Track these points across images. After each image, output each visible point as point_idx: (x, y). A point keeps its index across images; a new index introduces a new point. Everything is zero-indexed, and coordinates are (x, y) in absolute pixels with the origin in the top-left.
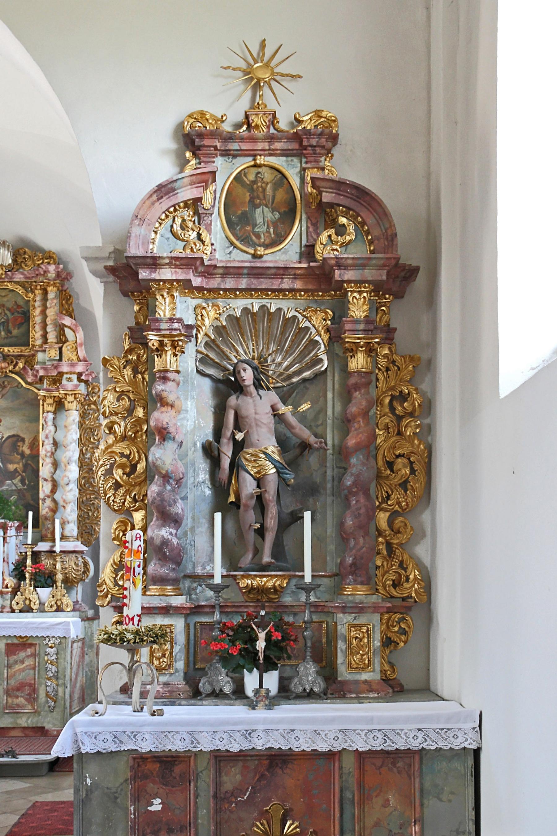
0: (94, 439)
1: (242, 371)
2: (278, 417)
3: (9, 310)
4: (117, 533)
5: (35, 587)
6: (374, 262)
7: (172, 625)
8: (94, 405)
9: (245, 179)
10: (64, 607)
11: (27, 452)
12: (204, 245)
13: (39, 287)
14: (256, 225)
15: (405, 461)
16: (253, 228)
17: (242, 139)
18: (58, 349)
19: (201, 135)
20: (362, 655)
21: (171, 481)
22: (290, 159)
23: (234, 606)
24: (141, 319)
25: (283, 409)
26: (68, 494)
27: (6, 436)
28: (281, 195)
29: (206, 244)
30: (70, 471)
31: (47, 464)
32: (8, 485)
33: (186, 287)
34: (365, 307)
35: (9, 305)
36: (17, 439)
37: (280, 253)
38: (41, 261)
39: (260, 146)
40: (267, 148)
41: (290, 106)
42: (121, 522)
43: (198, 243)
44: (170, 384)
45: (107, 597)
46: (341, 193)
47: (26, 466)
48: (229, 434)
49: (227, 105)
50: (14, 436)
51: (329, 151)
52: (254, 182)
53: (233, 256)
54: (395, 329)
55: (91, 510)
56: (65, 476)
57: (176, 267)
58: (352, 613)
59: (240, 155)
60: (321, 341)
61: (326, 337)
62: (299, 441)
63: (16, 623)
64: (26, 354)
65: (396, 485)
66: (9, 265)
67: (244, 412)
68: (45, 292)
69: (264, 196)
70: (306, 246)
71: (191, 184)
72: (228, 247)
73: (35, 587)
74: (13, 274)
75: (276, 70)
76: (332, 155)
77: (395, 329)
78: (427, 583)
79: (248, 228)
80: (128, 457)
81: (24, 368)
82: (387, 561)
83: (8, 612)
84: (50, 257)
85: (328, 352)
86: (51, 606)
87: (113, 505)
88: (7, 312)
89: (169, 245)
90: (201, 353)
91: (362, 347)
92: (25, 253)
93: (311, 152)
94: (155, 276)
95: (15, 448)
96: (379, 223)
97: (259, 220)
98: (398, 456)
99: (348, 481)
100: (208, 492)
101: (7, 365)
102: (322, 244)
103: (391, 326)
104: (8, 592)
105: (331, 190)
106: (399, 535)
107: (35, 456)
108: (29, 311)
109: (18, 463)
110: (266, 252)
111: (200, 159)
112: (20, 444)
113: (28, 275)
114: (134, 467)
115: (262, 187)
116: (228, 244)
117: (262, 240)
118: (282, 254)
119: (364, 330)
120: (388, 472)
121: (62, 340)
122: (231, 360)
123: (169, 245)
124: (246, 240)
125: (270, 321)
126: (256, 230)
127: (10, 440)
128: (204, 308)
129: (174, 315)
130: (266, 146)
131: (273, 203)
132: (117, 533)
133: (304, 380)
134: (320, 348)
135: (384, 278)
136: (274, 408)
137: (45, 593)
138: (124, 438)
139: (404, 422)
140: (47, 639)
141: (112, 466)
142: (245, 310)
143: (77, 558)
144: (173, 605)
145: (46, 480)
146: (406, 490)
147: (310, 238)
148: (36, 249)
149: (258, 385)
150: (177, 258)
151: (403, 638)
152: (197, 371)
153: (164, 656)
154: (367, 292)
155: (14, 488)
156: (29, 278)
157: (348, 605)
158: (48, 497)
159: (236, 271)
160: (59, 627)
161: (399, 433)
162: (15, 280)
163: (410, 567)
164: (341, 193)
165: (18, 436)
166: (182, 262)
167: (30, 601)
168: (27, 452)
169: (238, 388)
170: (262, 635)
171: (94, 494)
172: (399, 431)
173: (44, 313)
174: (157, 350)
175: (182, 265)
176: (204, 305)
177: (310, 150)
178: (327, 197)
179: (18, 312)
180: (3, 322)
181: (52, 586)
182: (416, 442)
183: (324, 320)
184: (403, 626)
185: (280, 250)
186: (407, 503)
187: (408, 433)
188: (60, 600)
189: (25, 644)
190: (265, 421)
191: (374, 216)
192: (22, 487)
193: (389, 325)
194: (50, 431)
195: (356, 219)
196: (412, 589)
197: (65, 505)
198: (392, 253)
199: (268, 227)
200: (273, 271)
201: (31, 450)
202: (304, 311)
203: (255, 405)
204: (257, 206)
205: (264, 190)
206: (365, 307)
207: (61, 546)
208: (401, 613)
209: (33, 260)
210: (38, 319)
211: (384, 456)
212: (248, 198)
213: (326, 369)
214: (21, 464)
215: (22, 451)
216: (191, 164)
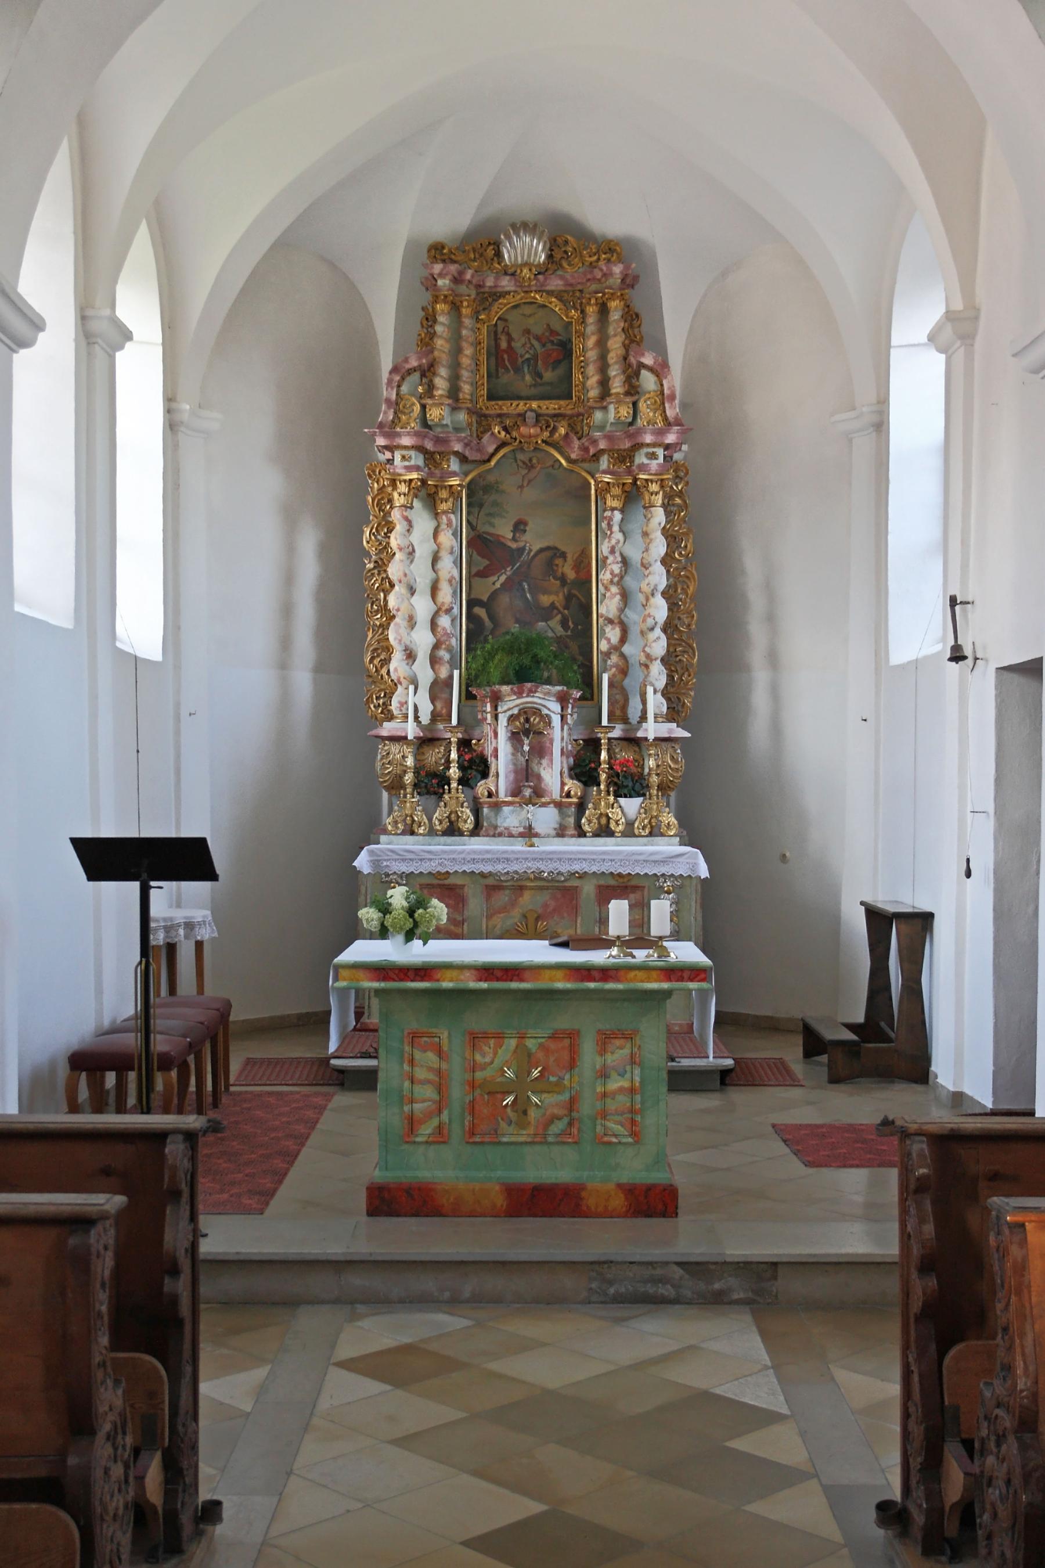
0: (680, 554)
3: (538, 338)
5: (617, 795)
8: (680, 497)
10: (663, 829)
11: (571, 575)
13: (593, 301)
18: (631, 406)
26: (654, 644)
27: (536, 548)
30: (657, 607)
35: (538, 330)
36: (554, 554)
38: (595, 258)
47: (569, 598)
50: (548, 548)
55: (677, 671)
56: (649, 615)
63: (613, 852)
64: (569, 412)
66: (539, 265)
68: (604, 310)
73: (617, 795)
74: (546, 279)
81: (567, 434)
83: (572, 836)
84: (611, 251)
86: (644, 828)
88: (535, 343)
92: (566, 242)
95: (550, 567)
104: (570, 804)
107: (584, 584)
108: (570, 341)
109: (557, 594)
112: (559, 561)
113: (573, 281)
121: (633, 390)
127: (543, 555)
137: (631, 805)
140: (662, 880)
148: (585, 236)
156: (571, 285)
160: (680, 859)
162: (549, 288)
165: (556, 548)
167: (609, 818)
168: (571, 575)
171: (680, 645)
173: (602, 344)
179: (552, 342)
180: (528, 359)
181: (644, 795)
188: (656, 817)
189: (626, 887)
192: (564, 633)
194: (618, 542)
197: (648, 663)
201: (577, 572)
207: (655, 731)
209: (581, 256)
210: (592, 355)
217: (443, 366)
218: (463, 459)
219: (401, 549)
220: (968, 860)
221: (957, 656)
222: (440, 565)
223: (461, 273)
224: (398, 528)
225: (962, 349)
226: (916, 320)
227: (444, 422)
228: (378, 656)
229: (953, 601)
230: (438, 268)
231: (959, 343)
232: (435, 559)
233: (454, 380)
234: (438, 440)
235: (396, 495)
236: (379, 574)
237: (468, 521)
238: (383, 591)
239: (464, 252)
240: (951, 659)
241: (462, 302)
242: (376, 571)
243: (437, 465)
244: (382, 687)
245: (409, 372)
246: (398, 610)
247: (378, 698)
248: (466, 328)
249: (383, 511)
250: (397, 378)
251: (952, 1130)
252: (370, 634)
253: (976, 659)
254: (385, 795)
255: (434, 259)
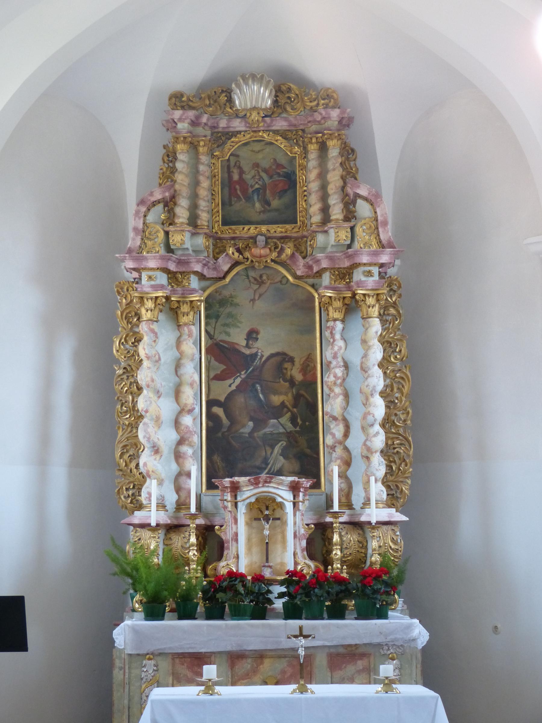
3: (265, 171)
8: (394, 307)
13: (314, 140)
18: (349, 230)
26: (373, 439)
31: (337, 396)
32: (273, 426)
35: (266, 164)
47: (297, 398)
55: (395, 462)
68: (323, 148)
81: (293, 255)
84: (329, 97)
92: (289, 90)
101: (268, 251)
108: (294, 173)
109: (286, 394)
112: (287, 365)
127: (273, 360)
143: (395, 533)
145: (335, 419)
148: (305, 84)
155: (282, 430)
156: (295, 126)
158: (340, 443)
162: (274, 128)
165: (284, 354)
168: (299, 377)
179: (279, 175)
180: (257, 189)
194: (340, 348)
201: (304, 375)
209: (303, 101)
210: (314, 186)
214: (290, 395)
215: (291, 376)
217: (183, 197)
218: (201, 277)
219: (148, 358)
222: (182, 371)
223: (198, 117)
224: (145, 338)
227: (185, 246)
228: (127, 452)
230: (177, 114)
232: (178, 366)
233: (194, 208)
234: (180, 262)
235: (143, 311)
236: (128, 379)
237: (206, 331)
238: (131, 393)
239: (201, 98)
241: (199, 142)
242: (125, 377)
243: (179, 283)
244: (131, 479)
245: (154, 204)
246: (146, 411)
247: (127, 489)
248: (203, 164)
249: (131, 323)
250: (143, 209)
252: (120, 433)
255: (175, 107)
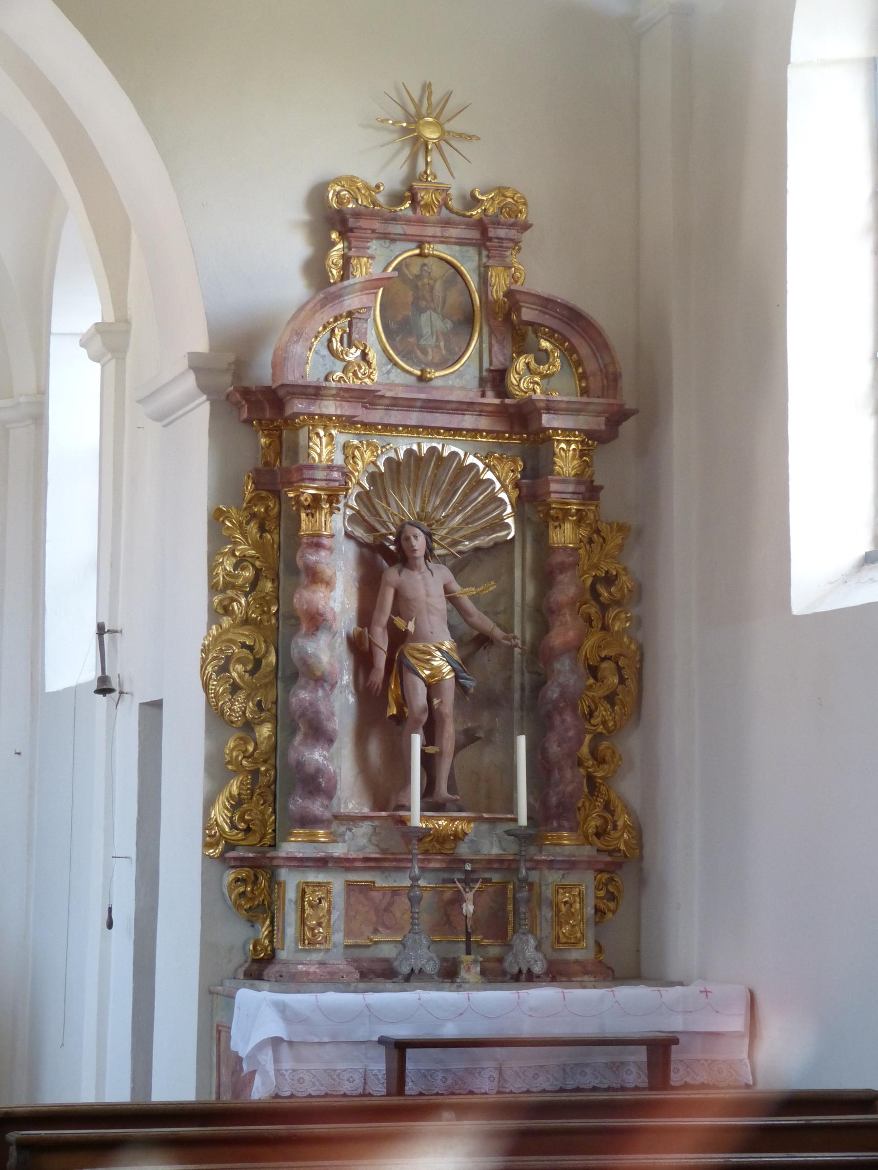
1: (412, 538)
2: (452, 599)
4: (234, 754)
6: (592, 407)
7: (329, 883)
9: (406, 271)
12: (370, 367)
14: (422, 336)
15: (613, 665)
16: (418, 340)
17: (408, 221)
19: (357, 214)
20: (573, 926)
21: (326, 685)
22: (465, 248)
23: (395, 860)
24: (271, 457)
25: (455, 586)
28: (454, 297)
29: (373, 366)
33: (347, 422)
34: (575, 462)
37: (453, 376)
39: (430, 231)
40: (439, 234)
41: (460, 174)
42: (241, 739)
43: (364, 367)
44: (323, 553)
45: (218, 845)
46: (548, 311)
48: (384, 620)
49: (374, 166)
51: (516, 242)
52: (419, 277)
53: (392, 377)
54: (601, 488)
57: (343, 399)
58: (560, 869)
59: (400, 240)
60: (507, 500)
61: (515, 494)
62: (476, 633)
65: (600, 698)
67: (410, 593)
69: (433, 300)
70: (489, 371)
71: (361, 291)
72: (387, 365)
75: (447, 127)
76: (520, 249)
77: (601, 488)
78: (638, 832)
79: (412, 340)
80: (251, 648)
82: (590, 800)
85: (518, 514)
87: (230, 715)
89: (325, 365)
90: (352, 508)
91: (572, 516)
93: (497, 244)
94: (314, 409)
96: (595, 355)
97: (426, 330)
98: (603, 659)
99: (553, 692)
100: (352, 699)
102: (518, 373)
103: (595, 484)
105: (535, 307)
106: (606, 766)
110: (437, 374)
111: (350, 243)
114: (258, 663)
115: (428, 284)
116: (385, 360)
117: (430, 358)
118: (456, 378)
119: (574, 493)
120: (591, 681)
122: (381, 517)
123: (325, 365)
124: (407, 356)
125: (437, 466)
126: (423, 342)
128: (357, 447)
129: (332, 460)
130: (438, 231)
131: (443, 308)
132: (234, 754)
133: (477, 549)
134: (505, 510)
135: (603, 427)
136: (447, 590)
138: (246, 621)
139: (612, 613)
141: (228, 659)
142: (409, 452)
144: (336, 855)
146: (613, 705)
147: (494, 359)
149: (429, 553)
150: (347, 390)
151: (612, 905)
152: (346, 532)
153: (319, 924)
154: (576, 442)
157: (558, 858)
159: (406, 403)
161: (605, 628)
163: (619, 810)
164: (548, 311)
166: (351, 394)
169: (402, 558)
170: (469, 896)
172: (603, 623)
174: (309, 507)
175: (351, 397)
176: (356, 442)
177: (495, 243)
178: (528, 314)
182: (625, 640)
183: (512, 471)
184: (611, 889)
185: (454, 372)
186: (615, 722)
187: (616, 629)
190: (439, 607)
191: (589, 345)
193: (592, 481)
195: (563, 345)
196: (622, 840)
198: (615, 398)
199: (437, 340)
200: (454, 406)
202: (486, 458)
203: (426, 585)
204: (421, 311)
205: (432, 289)
206: (575, 462)
208: (609, 872)
211: (586, 659)
212: (410, 299)
213: (513, 538)
216: (336, 248)
220: (110, 910)
221: (104, 688)
225: (114, 361)
226: (78, 308)
229: (101, 630)
231: (109, 356)
240: (98, 691)
251: (6, 1113)
253: (121, 693)
254: (419, 373)
